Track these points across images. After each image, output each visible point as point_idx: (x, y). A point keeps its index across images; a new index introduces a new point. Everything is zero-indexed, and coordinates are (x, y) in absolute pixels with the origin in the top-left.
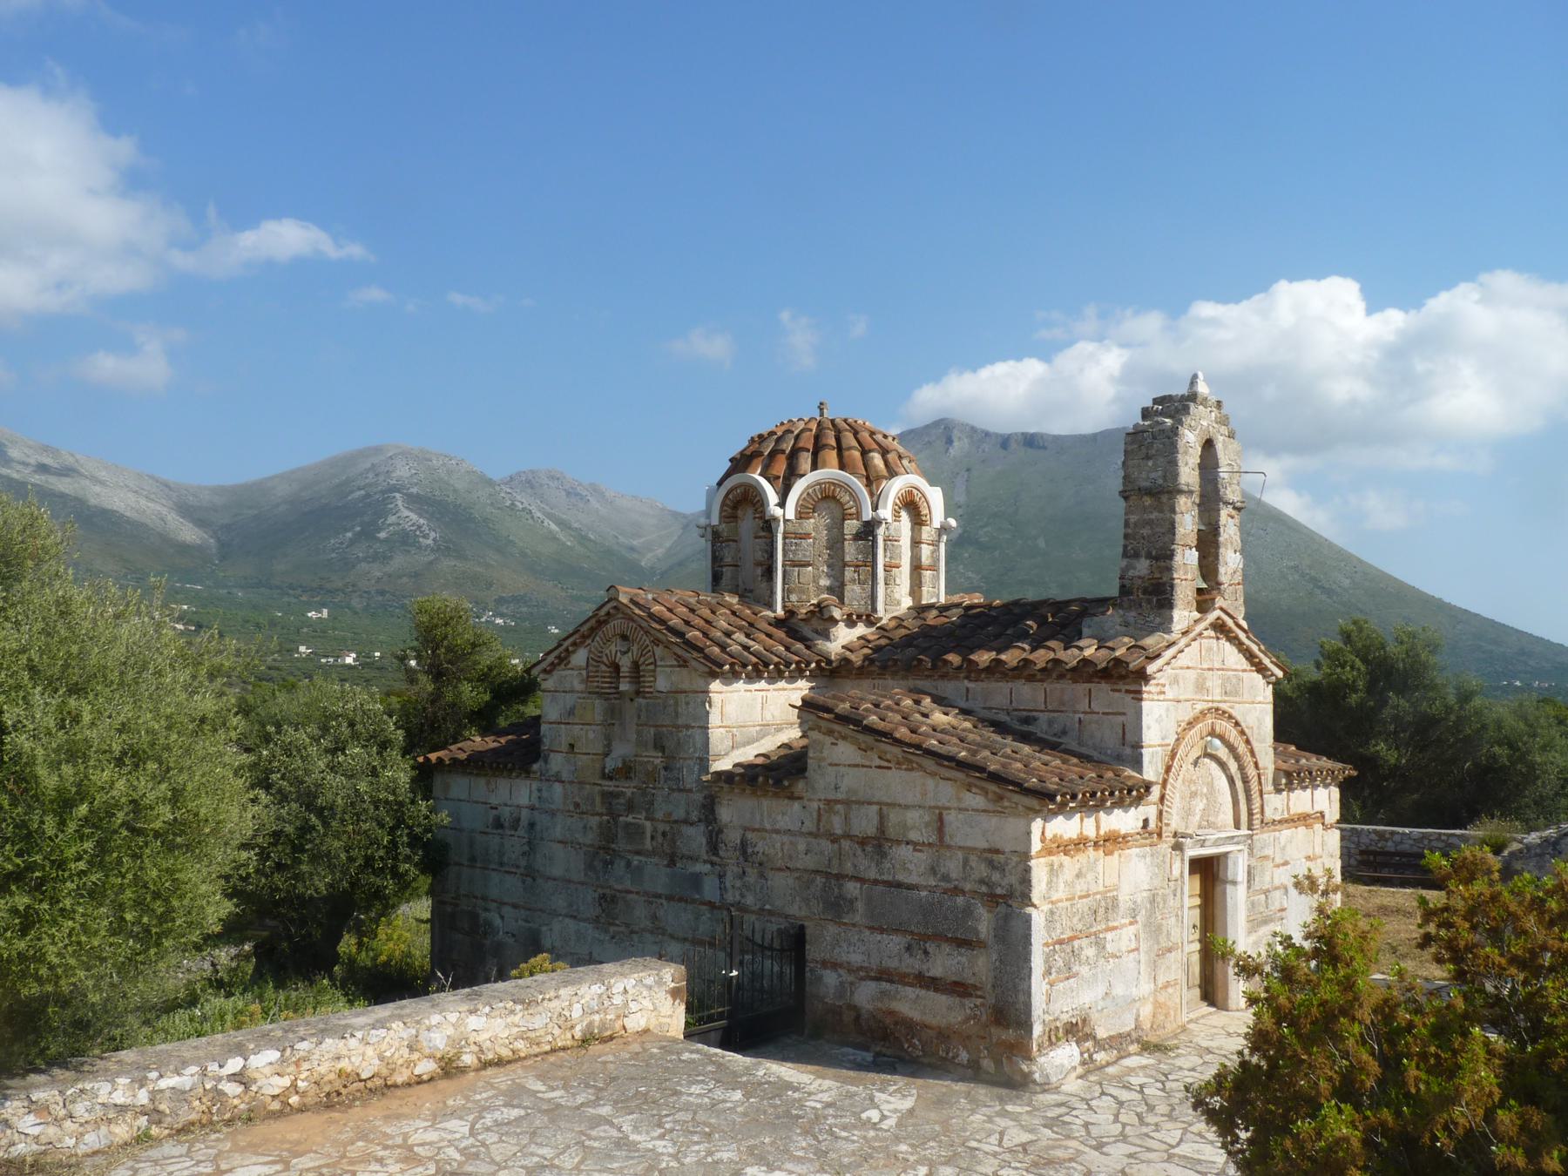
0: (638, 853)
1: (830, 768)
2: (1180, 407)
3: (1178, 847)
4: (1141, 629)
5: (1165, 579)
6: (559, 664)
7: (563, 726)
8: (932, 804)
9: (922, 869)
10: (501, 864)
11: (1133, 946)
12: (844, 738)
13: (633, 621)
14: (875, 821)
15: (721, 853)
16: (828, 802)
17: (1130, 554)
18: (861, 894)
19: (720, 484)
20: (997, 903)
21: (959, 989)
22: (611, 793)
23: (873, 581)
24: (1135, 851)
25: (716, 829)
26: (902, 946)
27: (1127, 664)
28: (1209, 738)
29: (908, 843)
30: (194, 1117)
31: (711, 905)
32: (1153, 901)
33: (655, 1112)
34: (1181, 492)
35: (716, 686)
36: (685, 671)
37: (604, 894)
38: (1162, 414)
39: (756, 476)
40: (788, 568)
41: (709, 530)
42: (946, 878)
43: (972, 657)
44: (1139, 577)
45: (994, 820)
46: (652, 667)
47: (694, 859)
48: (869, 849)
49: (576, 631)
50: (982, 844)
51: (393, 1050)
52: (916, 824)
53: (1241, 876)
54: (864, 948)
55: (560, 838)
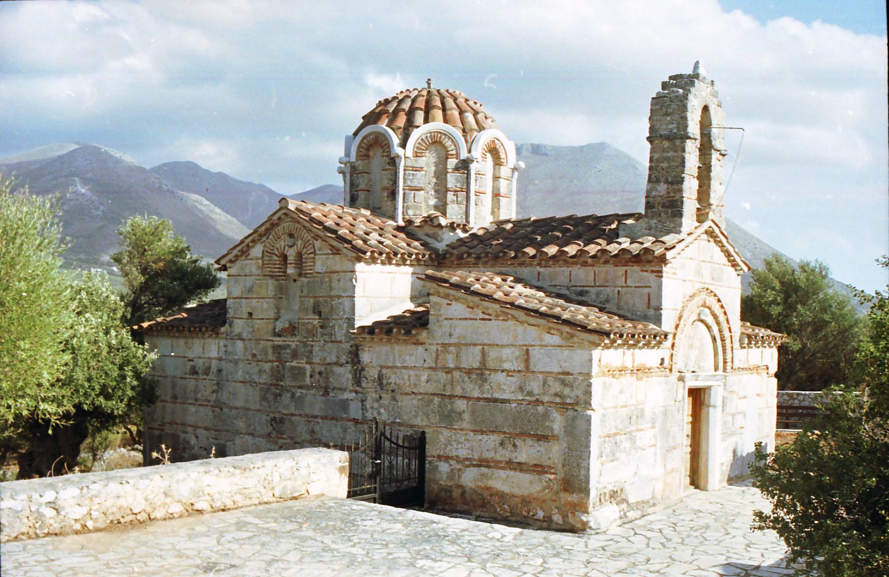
0: (300, 387)
1: (445, 321)
2: (688, 82)
3: (681, 379)
4: (661, 231)
5: (677, 197)
6: (241, 256)
7: (243, 300)
8: (521, 343)
9: (513, 389)
10: (197, 400)
11: (653, 443)
12: (457, 299)
13: (299, 222)
14: (479, 358)
15: (364, 385)
16: (444, 345)
17: (653, 180)
18: (467, 407)
19: (356, 134)
20: (567, 409)
21: (539, 469)
22: (280, 346)
23: (467, 202)
24: (655, 379)
25: (360, 368)
26: (497, 443)
27: (653, 251)
28: (702, 308)
29: (503, 371)
30: (24, 529)
31: (356, 421)
32: (665, 413)
33: (344, 534)
34: (689, 138)
35: (360, 267)
36: (337, 257)
37: (274, 417)
38: (676, 86)
39: (384, 126)
40: (407, 191)
41: (348, 165)
42: (530, 394)
43: (543, 249)
44: (660, 196)
45: (566, 352)
46: (312, 255)
47: (343, 390)
48: (473, 376)
49: (255, 231)
50: (556, 369)
51: (154, 495)
52: (510, 358)
53: (719, 403)
54: (469, 445)
55: (241, 379)
